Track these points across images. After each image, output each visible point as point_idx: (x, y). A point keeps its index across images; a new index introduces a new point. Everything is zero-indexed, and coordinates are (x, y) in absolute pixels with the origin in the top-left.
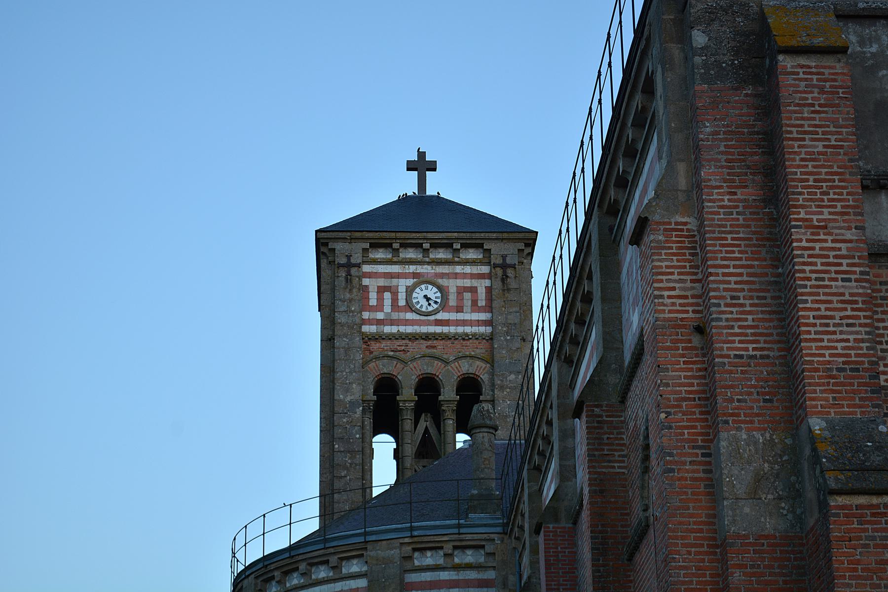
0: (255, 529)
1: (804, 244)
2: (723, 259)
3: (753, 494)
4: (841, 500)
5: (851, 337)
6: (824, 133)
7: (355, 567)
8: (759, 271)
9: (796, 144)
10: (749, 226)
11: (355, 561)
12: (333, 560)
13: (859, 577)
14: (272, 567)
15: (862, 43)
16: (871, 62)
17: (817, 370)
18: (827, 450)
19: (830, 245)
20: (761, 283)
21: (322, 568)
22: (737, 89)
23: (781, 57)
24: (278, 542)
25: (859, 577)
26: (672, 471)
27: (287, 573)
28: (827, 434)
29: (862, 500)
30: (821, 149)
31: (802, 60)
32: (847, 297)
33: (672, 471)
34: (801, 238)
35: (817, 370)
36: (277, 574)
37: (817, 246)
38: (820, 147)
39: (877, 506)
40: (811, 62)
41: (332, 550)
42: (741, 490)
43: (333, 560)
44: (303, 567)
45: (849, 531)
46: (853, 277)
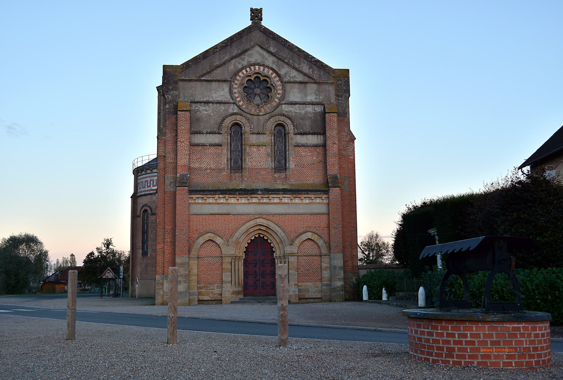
0: (140, 159)
1: (179, 145)
2: (168, 146)
3: (170, 185)
4: (178, 188)
5: (185, 160)
6: (184, 125)
7: (155, 171)
8: (174, 148)
9: (180, 127)
10: (173, 140)
11: (155, 169)
12: (151, 169)
13: (180, 200)
14: (139, 170)
15: (195, 107)
16: (196, 111)
17: (179, 166)
18: (178, 179)
19: (183, 145)
20: (174, 150)
21: (149, 170)
22: (173, 116)
23: (178, 112)
24: (140, 165)
25: (180, 200)
26: (159, 180)
27: (142, 171)
28: (179, 177)
29: (182, 188)
30: (184, 128)
31: (182, 112)
32: (185, 154)
33: (159, 180)
34: (179, 144)
35: (179, 166)
36: (140, 171)
37: (181, 145)
38: (183, 128)
39: (184, 189)
40: (183, 113)
41: (150, 167)
42: (168, 184)
43: (151, 169)
44: (145, 170)
45: (179, 193)
46: (187, 150)
